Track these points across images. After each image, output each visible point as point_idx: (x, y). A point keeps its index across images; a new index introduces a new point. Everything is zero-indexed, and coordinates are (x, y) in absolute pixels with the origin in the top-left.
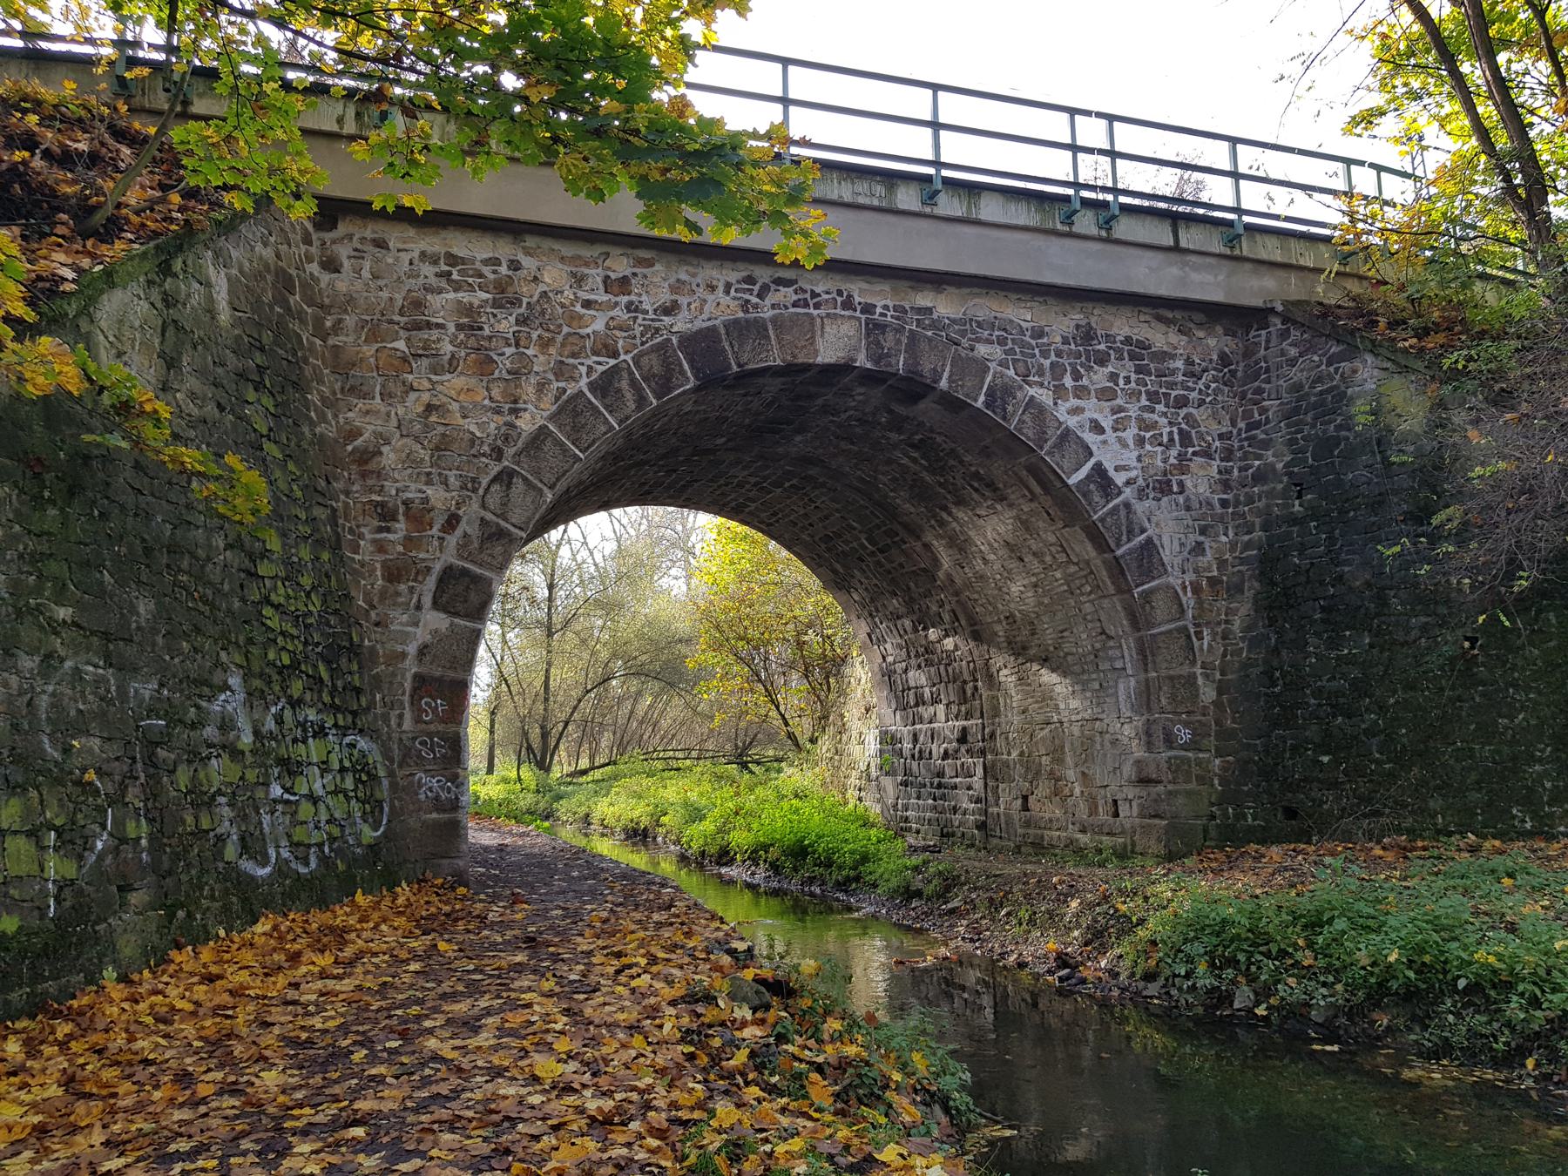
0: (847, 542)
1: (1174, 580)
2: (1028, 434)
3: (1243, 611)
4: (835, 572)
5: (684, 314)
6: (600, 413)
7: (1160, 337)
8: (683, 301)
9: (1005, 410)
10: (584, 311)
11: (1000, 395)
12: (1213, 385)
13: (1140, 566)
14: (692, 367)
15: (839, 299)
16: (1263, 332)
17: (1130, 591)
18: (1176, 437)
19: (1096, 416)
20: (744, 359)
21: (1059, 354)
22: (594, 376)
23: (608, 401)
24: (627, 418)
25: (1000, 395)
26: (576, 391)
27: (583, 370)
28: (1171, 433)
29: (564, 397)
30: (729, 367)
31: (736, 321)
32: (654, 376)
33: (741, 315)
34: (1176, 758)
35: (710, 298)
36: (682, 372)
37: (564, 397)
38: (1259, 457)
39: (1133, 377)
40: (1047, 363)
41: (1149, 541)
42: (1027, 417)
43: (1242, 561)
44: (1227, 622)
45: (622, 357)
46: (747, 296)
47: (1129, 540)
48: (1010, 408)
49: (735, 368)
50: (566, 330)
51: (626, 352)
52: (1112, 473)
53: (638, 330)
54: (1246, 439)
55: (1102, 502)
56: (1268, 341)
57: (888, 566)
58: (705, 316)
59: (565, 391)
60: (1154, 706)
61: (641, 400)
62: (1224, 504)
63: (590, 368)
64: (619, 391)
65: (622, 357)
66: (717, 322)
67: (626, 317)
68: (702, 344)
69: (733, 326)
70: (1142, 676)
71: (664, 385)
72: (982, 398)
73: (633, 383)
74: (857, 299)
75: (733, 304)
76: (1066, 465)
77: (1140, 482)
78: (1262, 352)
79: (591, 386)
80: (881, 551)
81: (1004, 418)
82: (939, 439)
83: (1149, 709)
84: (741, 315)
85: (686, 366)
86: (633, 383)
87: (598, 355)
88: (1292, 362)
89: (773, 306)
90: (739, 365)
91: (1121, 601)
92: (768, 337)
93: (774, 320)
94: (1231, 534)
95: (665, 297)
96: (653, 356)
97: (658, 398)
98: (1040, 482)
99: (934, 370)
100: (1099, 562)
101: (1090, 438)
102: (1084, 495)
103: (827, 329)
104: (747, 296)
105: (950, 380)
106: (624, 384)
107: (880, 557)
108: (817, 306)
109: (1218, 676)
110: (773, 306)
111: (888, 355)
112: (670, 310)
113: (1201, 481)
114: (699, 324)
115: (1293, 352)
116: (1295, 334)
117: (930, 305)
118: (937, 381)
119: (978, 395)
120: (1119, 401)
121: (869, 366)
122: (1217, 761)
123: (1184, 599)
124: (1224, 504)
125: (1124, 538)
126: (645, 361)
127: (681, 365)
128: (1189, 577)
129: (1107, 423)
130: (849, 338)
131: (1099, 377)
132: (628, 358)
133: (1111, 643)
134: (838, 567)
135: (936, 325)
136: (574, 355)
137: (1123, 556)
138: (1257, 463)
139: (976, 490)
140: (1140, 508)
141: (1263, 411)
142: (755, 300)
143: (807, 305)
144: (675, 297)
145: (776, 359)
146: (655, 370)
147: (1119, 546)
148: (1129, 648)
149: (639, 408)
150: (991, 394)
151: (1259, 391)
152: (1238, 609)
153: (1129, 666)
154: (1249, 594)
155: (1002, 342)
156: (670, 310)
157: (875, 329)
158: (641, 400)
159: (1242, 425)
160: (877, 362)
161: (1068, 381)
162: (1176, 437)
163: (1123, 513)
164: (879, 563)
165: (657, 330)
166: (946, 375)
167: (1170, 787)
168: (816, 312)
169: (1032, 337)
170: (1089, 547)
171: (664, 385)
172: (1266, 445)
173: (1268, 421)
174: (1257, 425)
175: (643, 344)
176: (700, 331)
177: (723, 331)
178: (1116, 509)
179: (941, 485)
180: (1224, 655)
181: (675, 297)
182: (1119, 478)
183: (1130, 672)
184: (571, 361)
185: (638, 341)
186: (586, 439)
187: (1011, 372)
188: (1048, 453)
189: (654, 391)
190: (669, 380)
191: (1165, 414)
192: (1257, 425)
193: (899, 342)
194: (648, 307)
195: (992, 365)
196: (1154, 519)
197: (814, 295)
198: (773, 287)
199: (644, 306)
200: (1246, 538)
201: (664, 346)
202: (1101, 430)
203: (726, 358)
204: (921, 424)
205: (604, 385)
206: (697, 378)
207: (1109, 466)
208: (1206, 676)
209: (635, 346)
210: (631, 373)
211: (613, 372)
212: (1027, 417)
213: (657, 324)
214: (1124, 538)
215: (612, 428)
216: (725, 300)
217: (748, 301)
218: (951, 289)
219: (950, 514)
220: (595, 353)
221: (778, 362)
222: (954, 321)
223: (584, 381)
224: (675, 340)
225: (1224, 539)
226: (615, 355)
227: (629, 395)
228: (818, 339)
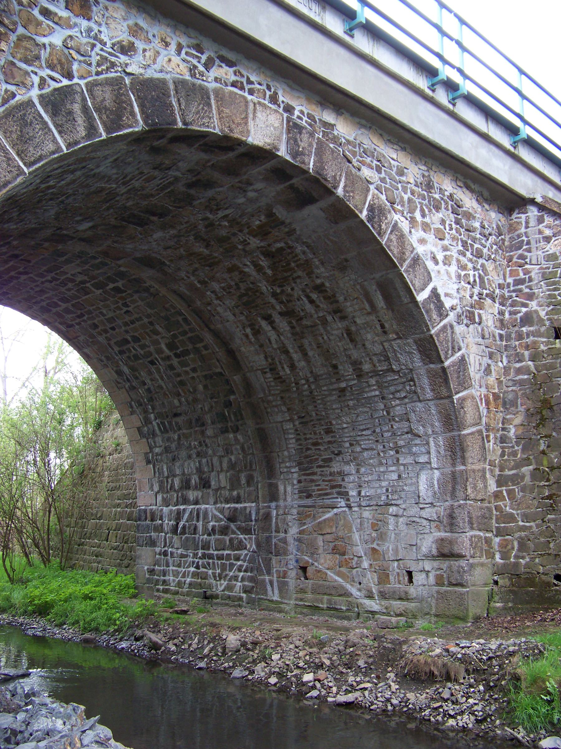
0: (143, 347)
1: (476, 394)
2: (394, 252)
3: (518, 420)
4: (119, 373)
5: (139, 58)
6: (50, 130)
7: (469, 202)
8: (140, 45)
9: (380, 226)
10: (41, 18)
11: (376, 212)
12: (495, 247)
13: (458, 377)
14: (142, 112)
15: (268, 93)
16: (523, 216)
17: (450, 397)
18: (477, 280)
19: (434, 249)
20: (189, 119)
21: (413, 193)
22: (46, 91)
23: (60, 119)
24: (76, 143)
25: (376, 212)
26: (25, 98)
27: (36, 80)
28: (474, 275)
29: (13, 102)
30: (175, 122)
31: (183, 82)
32: (106, 108)
33: (188, 77)
34: (475, 536)
35: (163, 52)
36: (133, 114)
37: (13, 102)
38: (525, 305)
39: (454, 226)
40: (406, 197)
41: (463, 357)
42: (393, 237)
43: (515, 383)
44: (503, 429)
45: (76, 81)
46: (195, 62)
47: (452, 355)
48: (383, 226)
49: (180, 125)
50: (21, 30)
51: (82, 77)
52: (443, 298)
53: (95, 59)
54: (514, 291)
55: (438, 319)
56: (527, 223)
57: (179, 370)
58: (157, 67)
59: (14, 96)
60: (460, 494)
61: (91, 130)
62: (501, 336)
63: (43, 80)
64: (70, 113)
65: (76, 81)
66: (168, 77)
67: (85, 40)
68: (152, 92)
69: (179, 84)
70: (448, 470)
71: (115, 120)
72: (365, 213)
73: (85, 109)
74: (281, 98)
75: (183, 66)
76: (417, 284)
77: (458, 309)
78: (523, 230)
79: (41, 97)
80: (177, 356)
81: (379, 234)
82: (299, 248)
83: (453, 495)
84: (188, 77)
85: (137, 109)
86: (85, 109)
87: (52, 70)
88: (547, 239)
89: (216, 80)
90: (185, 123)
91: (437, 406)
92: (209, 105)
93: (217, 92)
94: (505, 360)
95: (124, 37)
96: (108, 89)
97: (108, 131)
98: (387, 298)
99: (334, 177)
100: (422, 371)
101: (430, 264)
102: (427, 312)
103: (259, 114)
104: (195, 62)
105: (345, 190)
106: (77, 108)
107: (175, 362)
108: (251, 92)
109: (497, 472)
110: (216, 80)
111: (302, 154)
112: (127, 49)
113: (489, 314)
114: (150, 74)
115: (548, 232)
116: (548, 220)
117: (333, 122)
118: (336, 188)
119: (363, 208)
120: (446, 242)
121: (288, 158)
122: (497, 540)
123: (481, 408)
124: (501, 336)
125: (450, 352)
126: (98, 91)
127: (132, 107)
128: (484, 391)
129: (440, 257)
130: (275, 128)
131: (435, 218)
132: (82, 83)
133: (418, 441)
134: (126, 370)
135: (335, 140)
136: (26, 61)
137: (449, 367)
138: (524, 310)
139: (312, 302)
140: (459, 329)
141: (527, 272)
142: (201, 68)
143: (242, 88)
144: (132, 39)
145: (215, 127)
146: (108, 103)
147: (447, 358)
148: (437, 445)
149: (89, 136)
150: (371, 209)
151: (522, 257)
152: (512, 420)
153: (434, 460)
154: (522, 409)
155: (379, 170)
156: (127, 49)
157: (293, 128)
158: (91, 130)
159: (510, 280)
160: (294, 158)
161: (418, 215)
162: (477, 280)
163: (449, 331)
164: (171, 367)
165: (113, 65)
166: (342, 185)
167: (471, 561)
168: (250, 97)
169: (397, 174)
170: (417, 357)
171: (115, 120)
172: (531, 297)
173: (530, 280)
174: (522, 282)
175: (98, 74)
176: (151, 80)
177: (172, 87)
178: (445, 327)
179: (274, 295)
180: (503, 455)
181: (132, 39)
182: (448, 303)
183: (434, 465)
184: (23, 66)
185: (93, 69)
186: (33, 153)
187: (383, 197)
188: (406, 271)
189: (104, 124)
190: (120, 117)
191: (470, 260)
192: (522, 282)
193: (310, 145)
194: (106, 39)
195: (372, 187)
196: (465, 340)
197: (249, 82)
198: (217, 62)
199: (102, 37)
200: (518, 365)
201: (117, 83)
202: (437, 263)
203: (173, 111)
204: (291, 233)
205: (57, 102)
206: (145, 122)
207: (441, 291)
208: (491, 471)
209: (89, 74)
210: (84, 100)
211: (65, 93)
212: (393, 237)
213: (113, 59)
214: (450, 352)
215: (59, 149)
216: (176, 60)
217: (195, 67)
218: (347, 115)
219: (271, 322)
220: (51, 67)
221: (217, 131)
222: (349, 142)
223: (34, 93)
224: (127, 81)
225: (500, 364)
226: (70, 76)
227: (80, 120)
228: (251, 123)
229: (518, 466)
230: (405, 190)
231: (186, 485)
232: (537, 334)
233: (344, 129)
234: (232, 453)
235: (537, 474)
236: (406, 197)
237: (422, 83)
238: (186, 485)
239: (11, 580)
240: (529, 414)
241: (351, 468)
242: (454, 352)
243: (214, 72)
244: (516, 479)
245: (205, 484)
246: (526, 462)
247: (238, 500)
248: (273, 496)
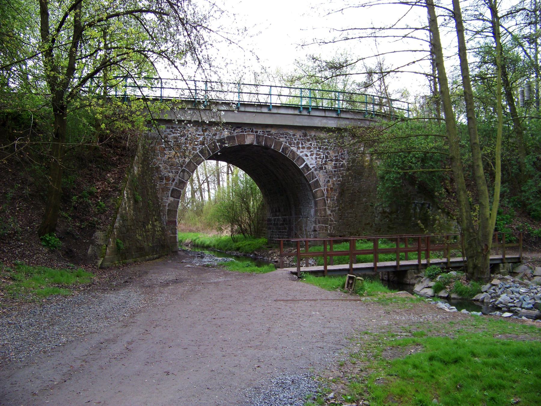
11: (285, 149)
25: (285, 149)
40: (296, 142)
52: (309, 166)
113: (330, 167)
158: (209, 154)
172: (344, 159)
207: (309, 164)
223: (198, 151)
229: (335, 207)
230: (295, 140)
231: (276, 211)
232: (343, 170)
233: (273, 131)
234: (530, 153)
235: (339, 210)
236: (296, 142)
237: (297, 112)
238: (276, 211)
239: (234, 242)
240: (339, 193)
241: (302, 207)
242: (313, 179)
243: (236, 131)
244: (334, 211)
245: (279, 211)
246: (337, 206)
247: (285, 215)
248: (291, 215)
